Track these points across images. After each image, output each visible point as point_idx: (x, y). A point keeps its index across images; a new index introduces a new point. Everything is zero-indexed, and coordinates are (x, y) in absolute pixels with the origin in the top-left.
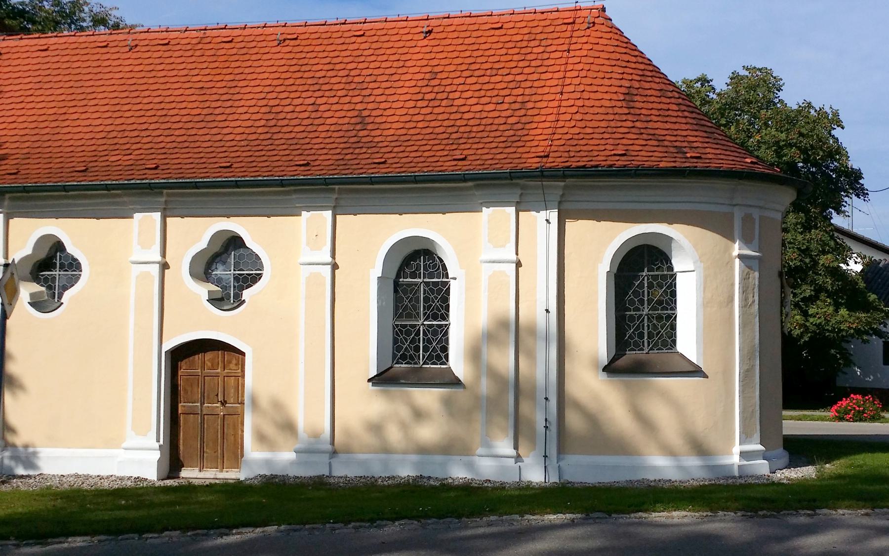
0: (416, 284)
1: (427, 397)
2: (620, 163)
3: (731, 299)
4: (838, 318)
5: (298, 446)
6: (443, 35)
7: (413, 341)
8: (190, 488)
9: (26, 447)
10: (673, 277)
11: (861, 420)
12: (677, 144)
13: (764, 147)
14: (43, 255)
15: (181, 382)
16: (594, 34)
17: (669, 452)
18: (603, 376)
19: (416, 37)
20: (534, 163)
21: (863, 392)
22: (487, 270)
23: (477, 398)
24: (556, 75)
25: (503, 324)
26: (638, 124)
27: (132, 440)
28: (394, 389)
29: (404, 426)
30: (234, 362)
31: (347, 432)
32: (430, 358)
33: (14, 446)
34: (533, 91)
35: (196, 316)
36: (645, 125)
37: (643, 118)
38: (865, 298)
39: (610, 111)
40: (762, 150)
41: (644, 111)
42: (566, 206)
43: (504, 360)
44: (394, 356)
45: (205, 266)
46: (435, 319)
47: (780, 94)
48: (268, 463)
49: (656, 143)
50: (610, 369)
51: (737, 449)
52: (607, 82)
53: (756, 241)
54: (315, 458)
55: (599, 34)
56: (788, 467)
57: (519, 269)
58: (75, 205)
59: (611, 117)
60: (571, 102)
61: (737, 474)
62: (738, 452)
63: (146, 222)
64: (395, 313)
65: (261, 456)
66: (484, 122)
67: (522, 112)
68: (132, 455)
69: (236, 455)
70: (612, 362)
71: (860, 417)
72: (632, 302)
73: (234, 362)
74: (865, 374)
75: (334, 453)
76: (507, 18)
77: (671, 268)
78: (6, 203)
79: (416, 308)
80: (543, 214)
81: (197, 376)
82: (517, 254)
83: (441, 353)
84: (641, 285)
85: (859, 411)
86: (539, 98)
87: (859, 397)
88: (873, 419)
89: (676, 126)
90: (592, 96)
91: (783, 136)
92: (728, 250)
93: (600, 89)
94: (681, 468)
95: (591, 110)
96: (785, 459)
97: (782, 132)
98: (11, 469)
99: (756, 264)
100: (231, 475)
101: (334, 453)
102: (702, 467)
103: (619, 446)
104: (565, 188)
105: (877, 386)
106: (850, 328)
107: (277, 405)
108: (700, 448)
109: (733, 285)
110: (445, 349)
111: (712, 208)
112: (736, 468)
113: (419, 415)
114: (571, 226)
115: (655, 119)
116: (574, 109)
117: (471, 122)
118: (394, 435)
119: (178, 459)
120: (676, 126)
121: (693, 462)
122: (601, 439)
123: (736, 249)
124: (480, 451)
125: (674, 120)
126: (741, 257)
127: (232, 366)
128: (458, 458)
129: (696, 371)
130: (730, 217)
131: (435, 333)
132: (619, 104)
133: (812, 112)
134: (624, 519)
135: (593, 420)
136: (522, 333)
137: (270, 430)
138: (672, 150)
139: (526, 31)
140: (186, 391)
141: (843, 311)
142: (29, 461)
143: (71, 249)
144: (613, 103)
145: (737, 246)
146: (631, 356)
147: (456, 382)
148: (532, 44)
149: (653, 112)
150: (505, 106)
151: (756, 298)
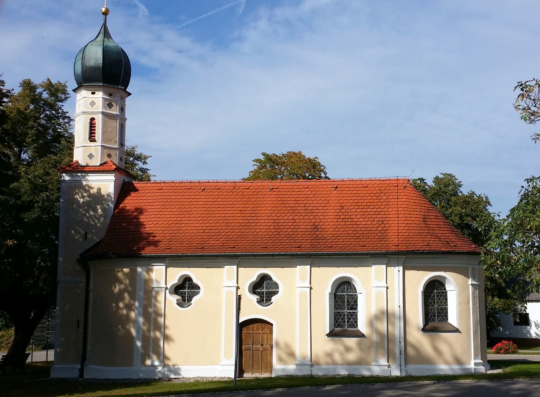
0: (344, 295)
1: (351, 342)
2: (427, 249)
3: (469, 302)
4: (494, 302)
5: (296, 362)
6: (343, 189)
7: (343, 319)
8: (248, 381)
9: (174, 366)
10: (446, 293)
11: (508, 353)
12: (446, 240)
13: (453, 215)
14: (180, 283)
15: (243, 337)
16: (406, 191)
17: (447, 363)
18: (421, 333)
19: (331, 189)
20: (394, 249)
21: (508, 339)
22: (375, 290)
23: (371, 342)
24: (394, 209)
25: (383, 313)
26: (430, 231)
27: (224, 361)
28: (336, 338)
29: (341, 354)
30: (266, 328)
31: (317, 357)
32: (350, 325)
33: (168, 365)
34: (386, 216)
35: (252, 309)
36: (433, 232)
37: (431, 228)
38: (506, 292)
39: (418, 226)
40: (453, 217)
41: (431, 226)
42: (405, 265)
43: (383, 327)
44: (335, 325)
45: (255, 288)
46: (352, 310)
47: (460, 188)
48: (284, 370)
49: (438, 240)
50: (424, 330)
51: (473, 362)
52: (415, 213)
53: (477, 278)
54: (304, 367)
55: (409, 192)
56: (491, 369)
57: (386, 290)
58: (199, 262)
59: (419, 228)
60: (403, 222)
61: (473, 372)
62: (473, 363)
63: (230, 270)
64: (335, 307)
65: (280, 367)
66: (368, 229)
67: (383, 225)
68: (223, 369)
69: (270, 368)
70: (424, 327)
71: (507, 352)
72: (431, 303)
73: (266, 328)
74: (505, 330)
75: (312, 365)
76: (368, 182)
77: (445, 289)
78: (167, 261)
79: (344, 305)
80: (397, 268)
81: (251, 335)
82: (166, 284)
83: (355, 324)
84: (434, 296)
85: (507, 349)
86: (389, 219)
87: (506, 342)
88: (513, 353)
89: (444, 232)
90: (411, 219)
91: (464, 211)
92: (467, 282)
93: (413, 216)
94: (452, 369)
95: (411, 225)
96: (489, 367)
97: (463, 209)
98: (168, 375)
99: (477, 287)
100: (266, 375)
101: (312, 365)
102: (460, 369)
103: (428, 361)
104: (405, 258)
105: (511, 337)
106: (500, 307)
107: (287, 346)
108: (459, 362)
109: (469, 296)
110: (356, 322)
111: (460, 265)
112: (473, 369)
113: (348, 349)
114: (407, 272)
115: (436, 229)
116: (404, 225)
117: (363, 229)
118: (337, 358)
119: (242, 369)
120: (444, 232)
121: (456, 367)
122: (422, 358)
123: (470, 281)
124: (373, 363)
125: (443, 229)
126: (472, 285)
127: (266, 329)
128: (364, 366)
129: (457, 331)
130: (467, 269)
131: (352, 315)
132: (421, 223)
133: (475, 197)
134: (451, 382)
135: (417, 349)
136: (389, 317)
137: (284, 356)
138: (445, 242)
139: (378, 189)
140: (245, 340)
141: (496, 299)
142: (176, 371)
143: (195, 281)
144: (419, 222)
145: (470, 280)
146: (431, 325)
147: (363, 336)
148: (382, 195)
149: (435, 226)
150: (376, 223)
151: (478, 301)
